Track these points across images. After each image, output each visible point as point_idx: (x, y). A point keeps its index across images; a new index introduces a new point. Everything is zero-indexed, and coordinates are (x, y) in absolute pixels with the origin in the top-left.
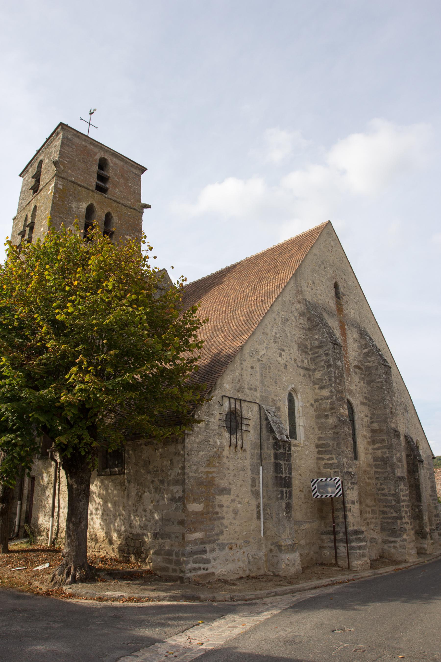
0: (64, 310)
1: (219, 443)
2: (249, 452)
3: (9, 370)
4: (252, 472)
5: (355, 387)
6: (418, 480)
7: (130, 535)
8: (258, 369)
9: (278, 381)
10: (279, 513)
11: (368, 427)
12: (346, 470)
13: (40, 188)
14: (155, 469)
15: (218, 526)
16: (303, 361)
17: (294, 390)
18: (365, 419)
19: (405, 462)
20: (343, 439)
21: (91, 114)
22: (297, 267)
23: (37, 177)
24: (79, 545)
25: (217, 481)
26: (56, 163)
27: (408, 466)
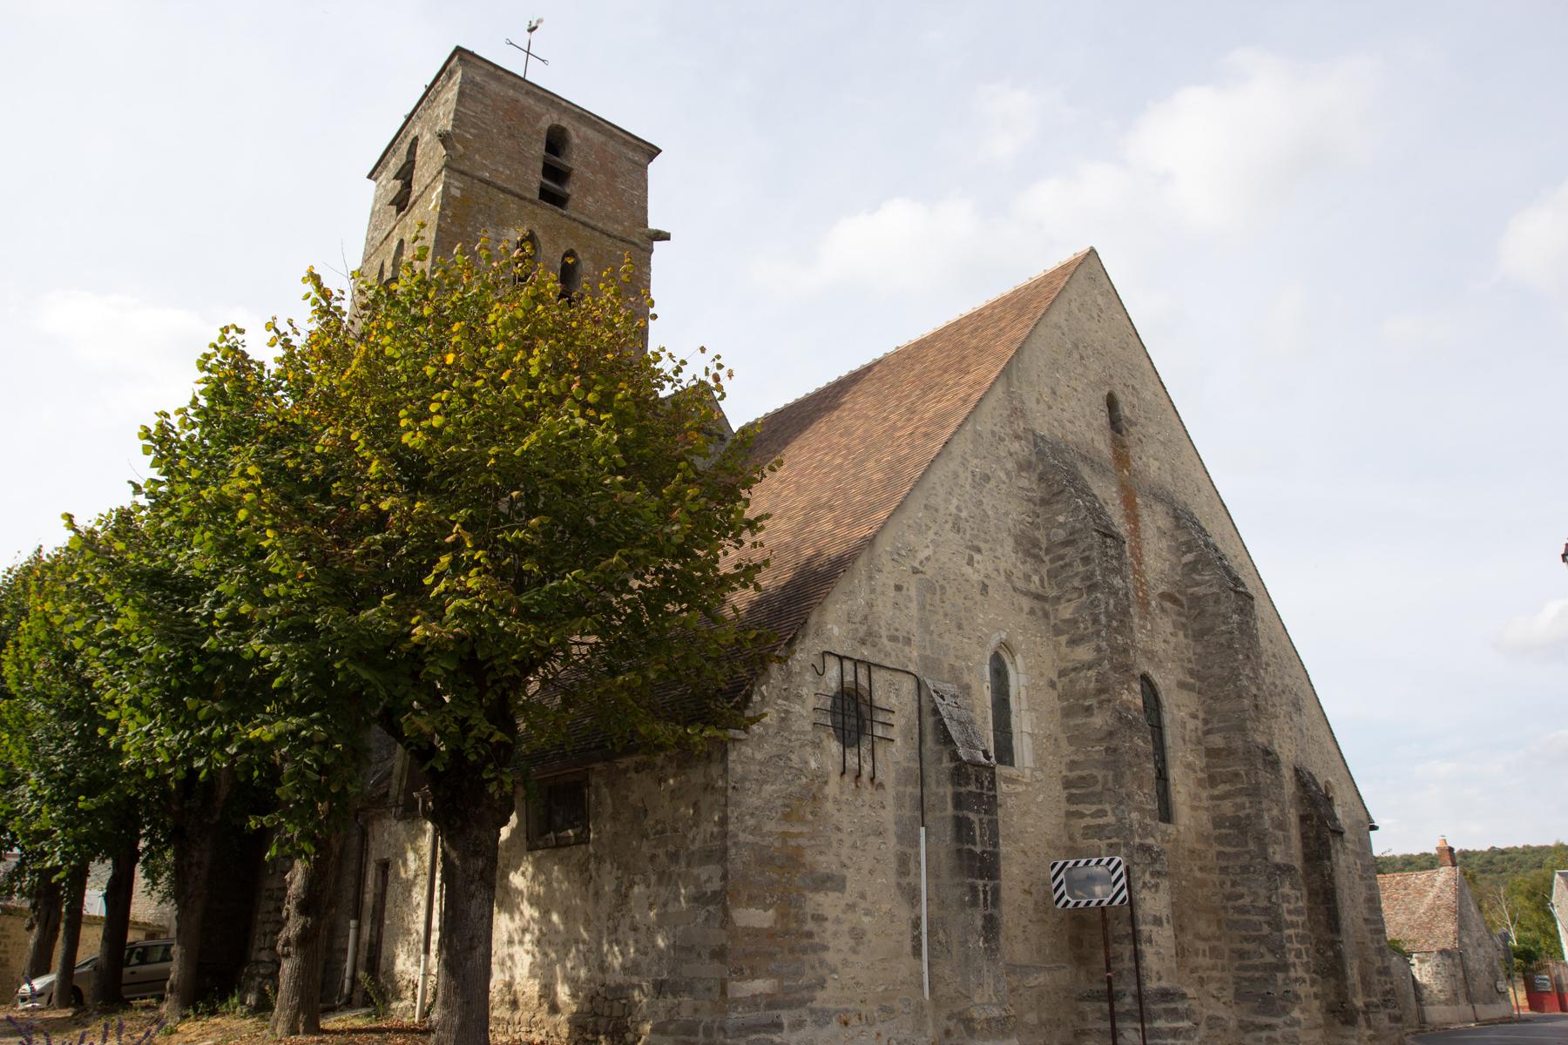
0: (424, 424)
1: (813, 765)
2: (890, 791)
3: (286, 561)
4: (900, 839)
5: (1161, 644)
6: (1331, 878)
7: (601, 990)
8: (913, 593)
9: (964, 622)
10: (967, 941)
11: (1199, 743)
12: (1137, 840)
13: (412, 200)
14: (659, 827)
15: (813, 968)
16: (1028, 578)
17: (1005, 645)
18: (1191, 724)
19: (1295, 833)
20: (1130, 766)
21: (531, 30)
22: (1011, 353)
23: (406, 175)
24: (468, 1003)
25: (809, 857)
26: (444, 138)
27: (1305, 845)
